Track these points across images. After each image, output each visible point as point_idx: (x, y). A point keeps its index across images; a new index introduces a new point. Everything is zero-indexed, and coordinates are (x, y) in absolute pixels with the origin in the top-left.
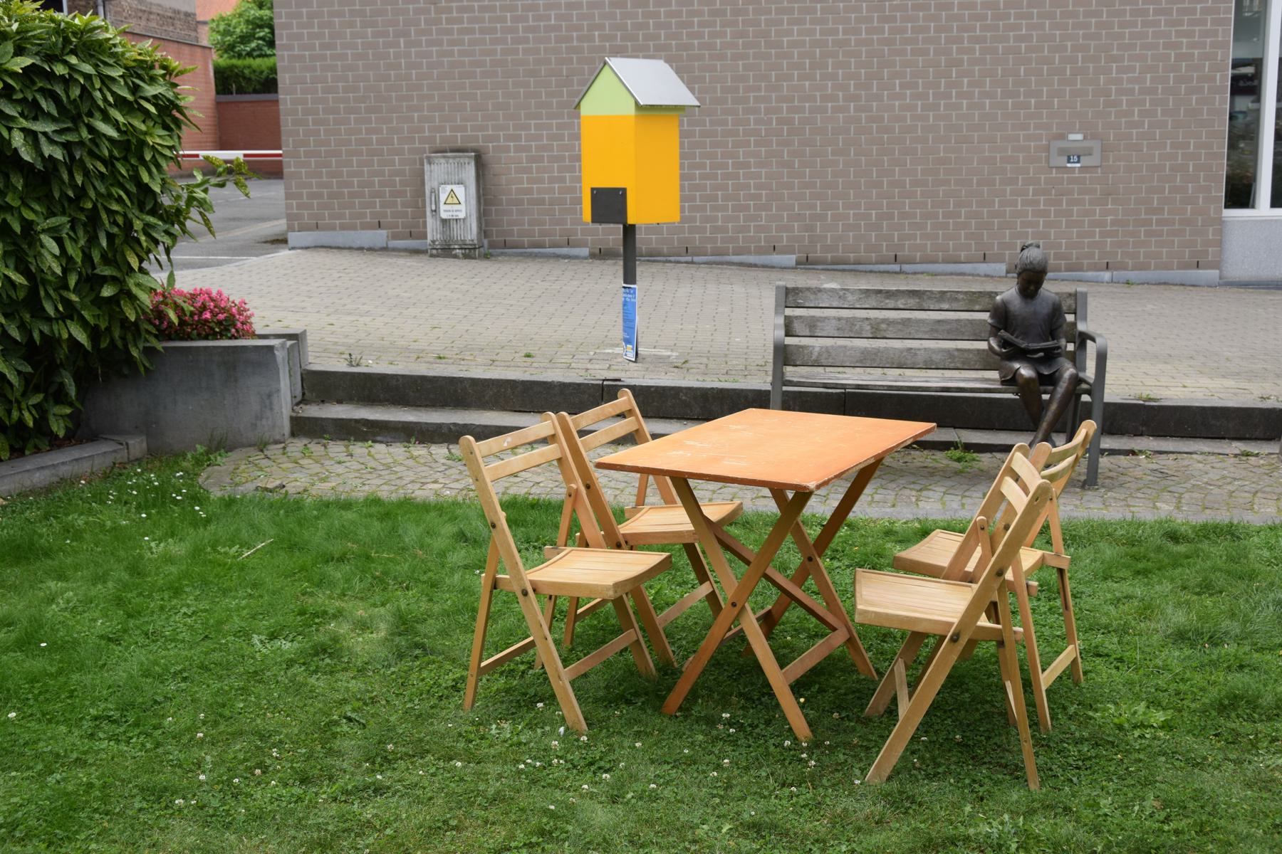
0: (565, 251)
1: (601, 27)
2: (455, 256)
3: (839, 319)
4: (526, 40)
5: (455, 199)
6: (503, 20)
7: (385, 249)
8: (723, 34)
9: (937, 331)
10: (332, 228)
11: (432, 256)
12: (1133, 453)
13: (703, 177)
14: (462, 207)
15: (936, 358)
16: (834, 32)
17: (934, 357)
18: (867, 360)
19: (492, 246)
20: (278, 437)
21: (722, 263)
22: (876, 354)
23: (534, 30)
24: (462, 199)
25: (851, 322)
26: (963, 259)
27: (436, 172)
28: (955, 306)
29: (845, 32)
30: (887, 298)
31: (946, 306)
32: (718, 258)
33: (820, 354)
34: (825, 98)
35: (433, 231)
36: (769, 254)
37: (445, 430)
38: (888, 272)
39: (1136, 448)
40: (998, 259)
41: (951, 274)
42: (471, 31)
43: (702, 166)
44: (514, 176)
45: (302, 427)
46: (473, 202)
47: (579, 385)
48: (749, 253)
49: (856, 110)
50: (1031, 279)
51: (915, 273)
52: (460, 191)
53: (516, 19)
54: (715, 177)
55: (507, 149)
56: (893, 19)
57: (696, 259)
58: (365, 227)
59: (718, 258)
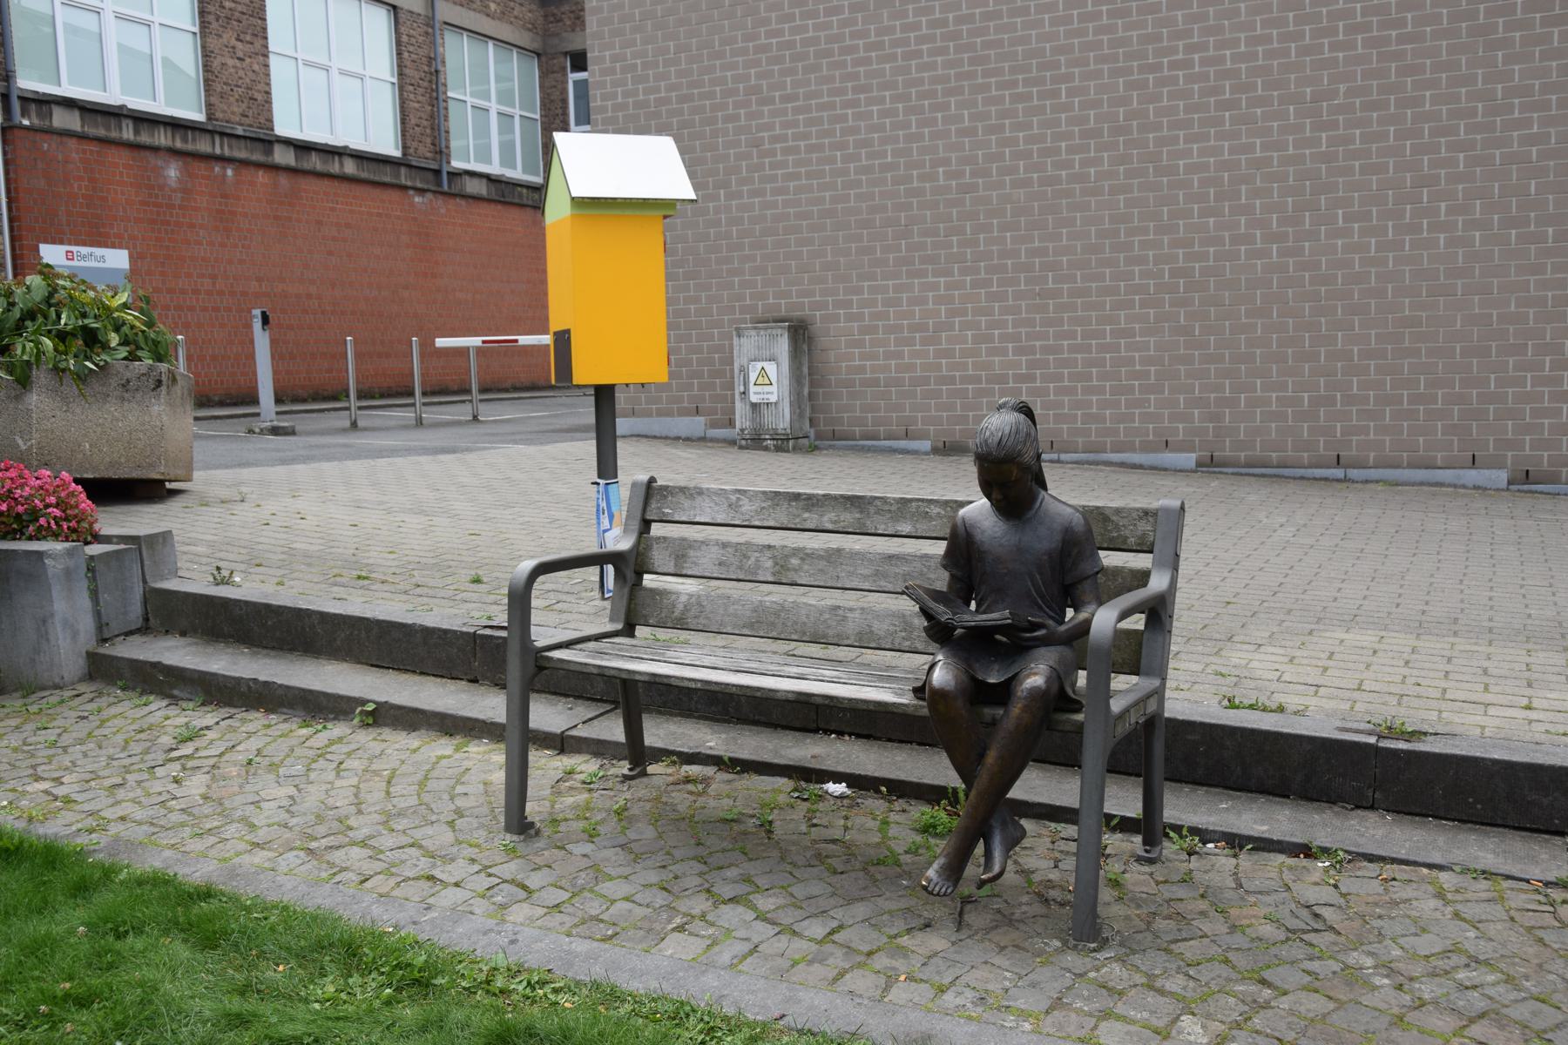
0: (903, 444)
1: (946, 162)
2: (766, 449)
3: (725, 545)
4: (858, 184)
5: (767, 379)
6: (832, 161)
7: (703, 439)
8: (1097, 161)
9: (885, 576)
10: (647, 414)
11: (741, 447)
12: (1305, 851)
13: (1074, 349)
14: (774, 389)
15: (880, 628)
16: (1250, 148)
17: (876, 626)
18: (767, 627)
19: (819, 436)
20: (57, 680)
21: (1097, 463)
22: (777, 614)
23: (867, 170)
24: (774, 381)
25: (742, 550)
26: (1439, 463)
27: (746, 346)
28: (922, 528)
29: (1265, 147)
30: (807, 510)
31: (906, 528)
32: (1092, 456)
33: (686, 608)
34: (1236, 240)
35: (742, 419)
36: (1162, 452)
37: (244, 689)
38: (1326, 479)
39: (1321, 838)
40: (922, 436)
41: (1422, 484)
42: (797, 176)
43: (1071, 335)
44: (843, 347)
45: (103, 671)
46: (786, 382)
47: (446, 631)
48: (1133, 450)
49: (1281, 254)
50: (1011, 478)
51: (1367, 482)
52: (771, 368)
53: (847, 159)
54: (1088, 349)
55: (836, 318)
56: (1334, 125)
57: (1063, 457)
58: (684, 413)
59: (1092, 456)
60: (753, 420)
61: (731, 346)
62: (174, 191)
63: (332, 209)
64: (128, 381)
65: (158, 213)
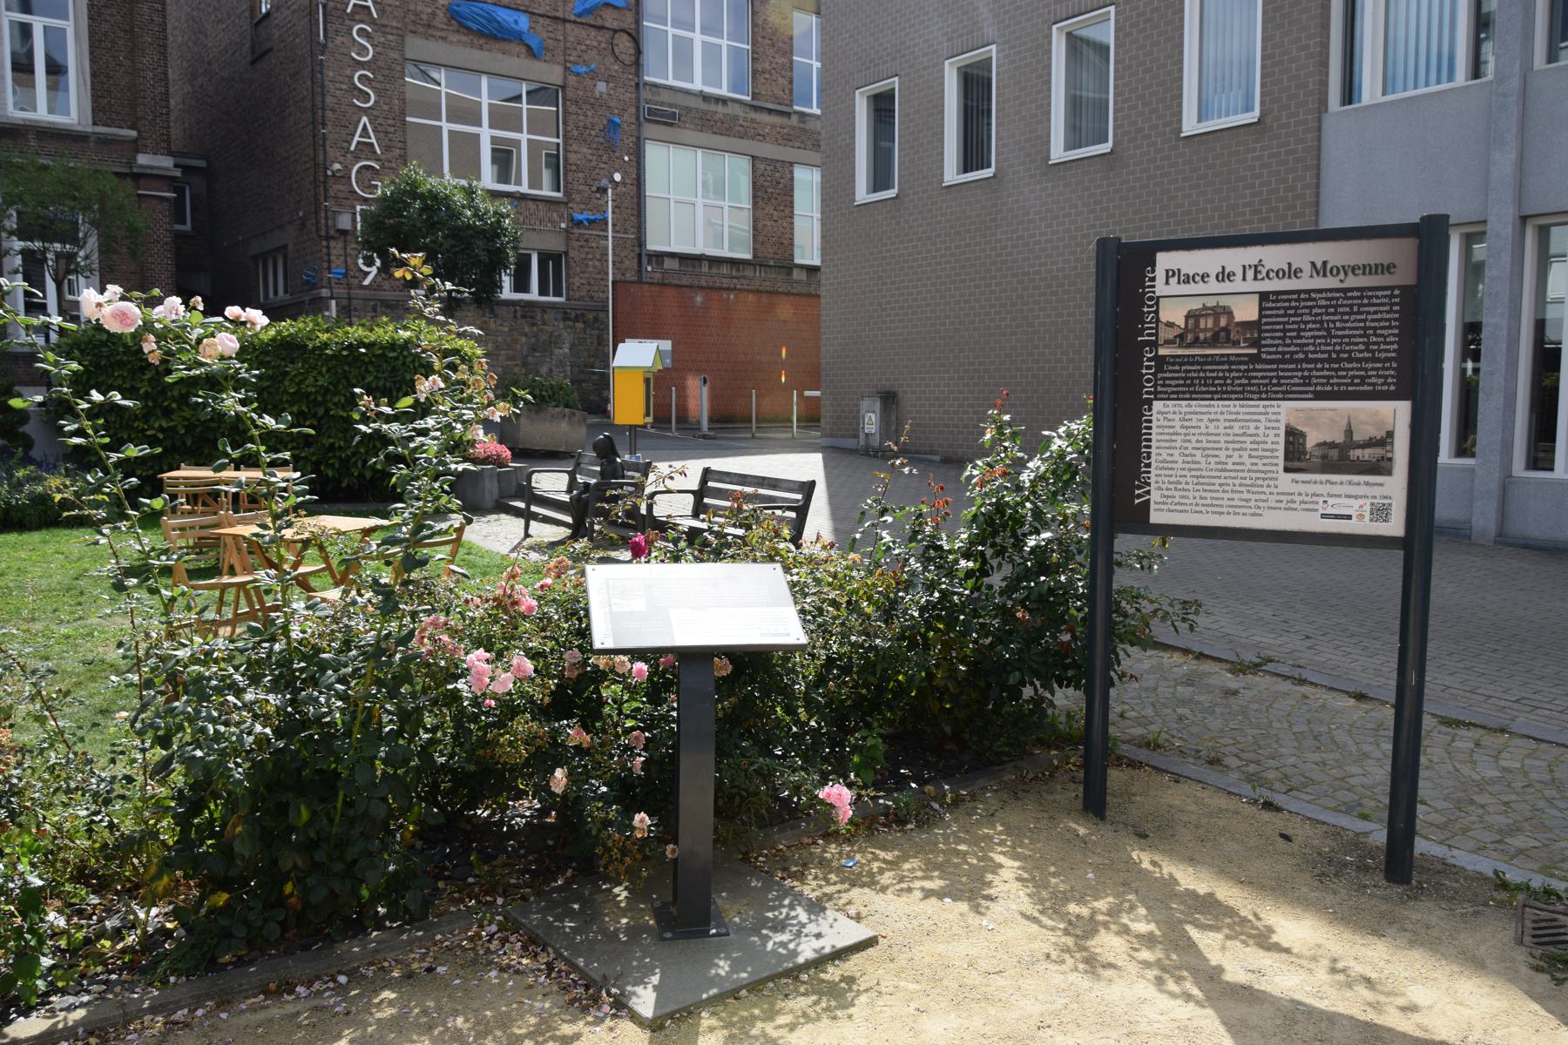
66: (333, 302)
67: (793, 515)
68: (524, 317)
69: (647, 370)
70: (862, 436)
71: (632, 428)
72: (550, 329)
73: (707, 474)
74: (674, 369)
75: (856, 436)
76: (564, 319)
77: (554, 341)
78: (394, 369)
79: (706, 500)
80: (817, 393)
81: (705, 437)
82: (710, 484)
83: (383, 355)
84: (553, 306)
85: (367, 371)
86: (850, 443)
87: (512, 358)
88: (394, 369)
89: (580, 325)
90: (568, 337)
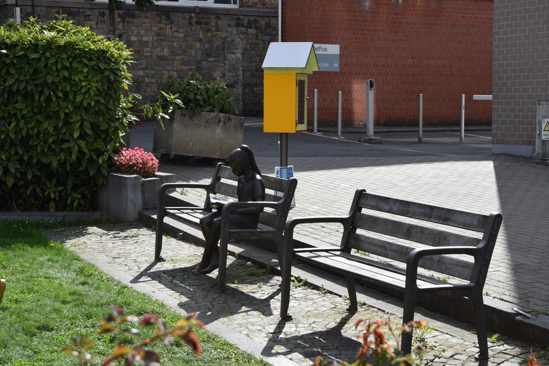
11: (537, 163)
60: (542, 149)
61: (536, 108)
62: (368, 13)
63: (463, 17)
64: (208, 120)
65: (358, 25)
66: (18, 9)
67: (470, 259)
68: (198, 23)
69: (299, 72)
70: (538, 143)
71: (284, 137)
72: (224, 35)
73: (361, 198)
74: (342, 73)
75: (531, 143)
76: (238, 25)
77: (227, 46)
78: (36, 71)
79: (359, 231)
80: (489, 97)
81: (370, 141)
82: (365, 211)
83: (25, 56)
84: (227, 13)
85: (8, 73)
86: (524, 150)
87: (188, 63)
88: (36, 71)
89: (252, 31)
90: (240, 43)
